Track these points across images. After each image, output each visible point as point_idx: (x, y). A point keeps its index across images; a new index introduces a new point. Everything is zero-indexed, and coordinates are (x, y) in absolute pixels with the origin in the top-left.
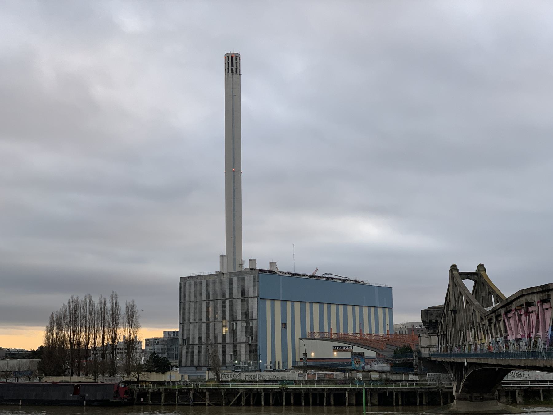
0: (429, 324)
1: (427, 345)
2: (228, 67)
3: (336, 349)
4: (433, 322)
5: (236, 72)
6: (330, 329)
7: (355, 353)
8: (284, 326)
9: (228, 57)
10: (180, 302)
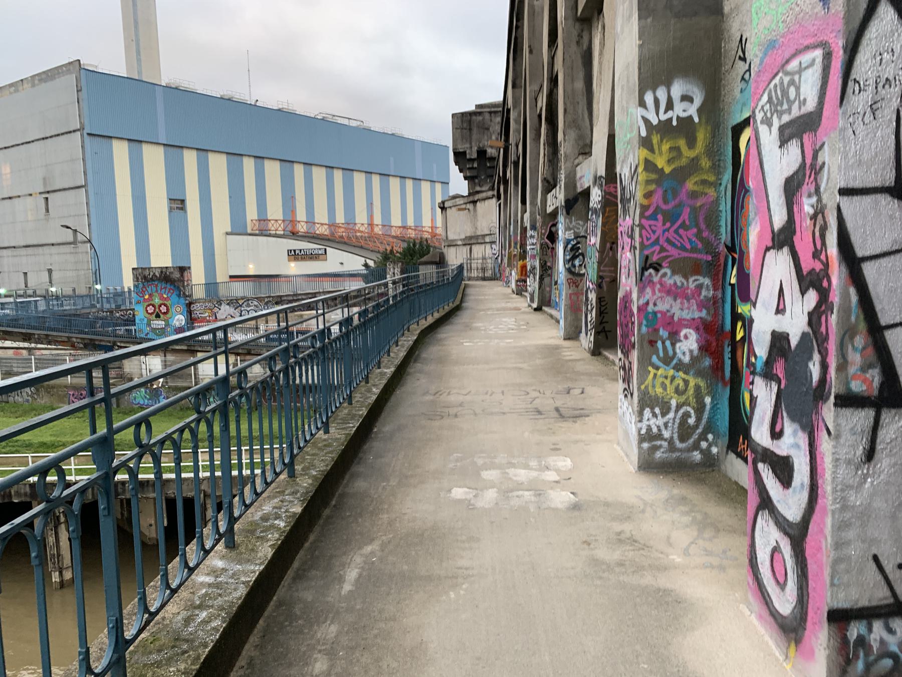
0: (475, 165)
1: (464, 237)
3: (294, 255)
4: (488, 155)
6: (371, 217)
7: (147, 272)
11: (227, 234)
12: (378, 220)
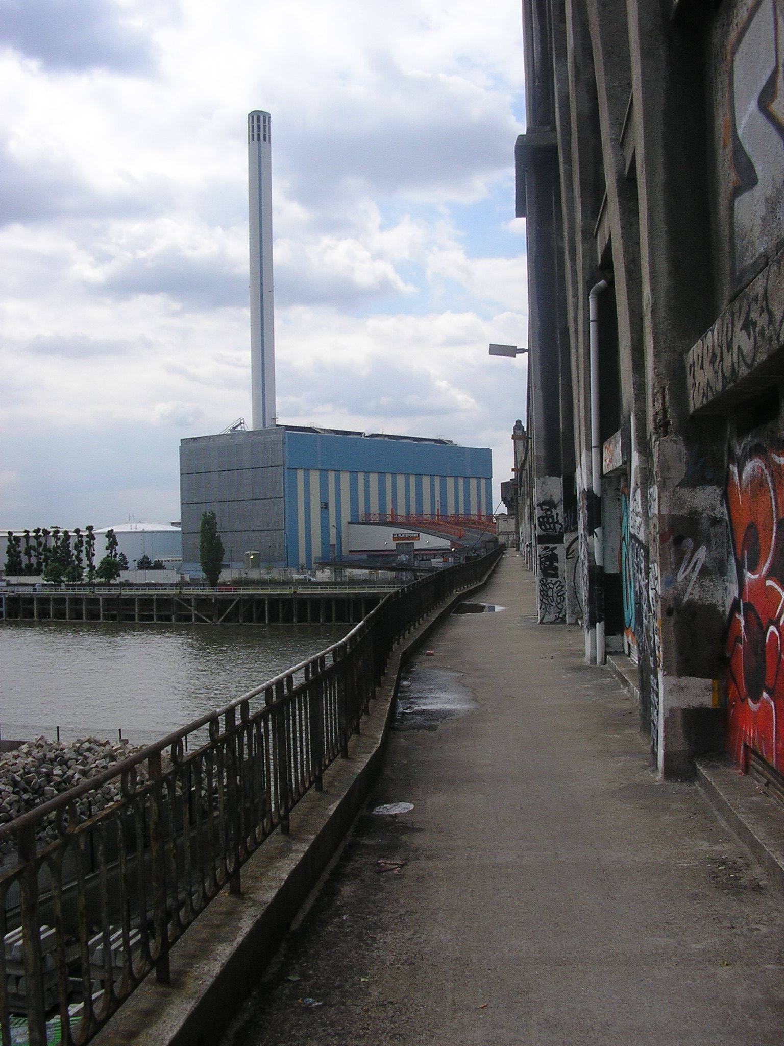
2: (253, 132)
5: (265, 140)
6: (479, 510)
8: (325, 506)
9: (253, 117)
10: (181, 474)
11: (349, 523)
12: (484, 513)
